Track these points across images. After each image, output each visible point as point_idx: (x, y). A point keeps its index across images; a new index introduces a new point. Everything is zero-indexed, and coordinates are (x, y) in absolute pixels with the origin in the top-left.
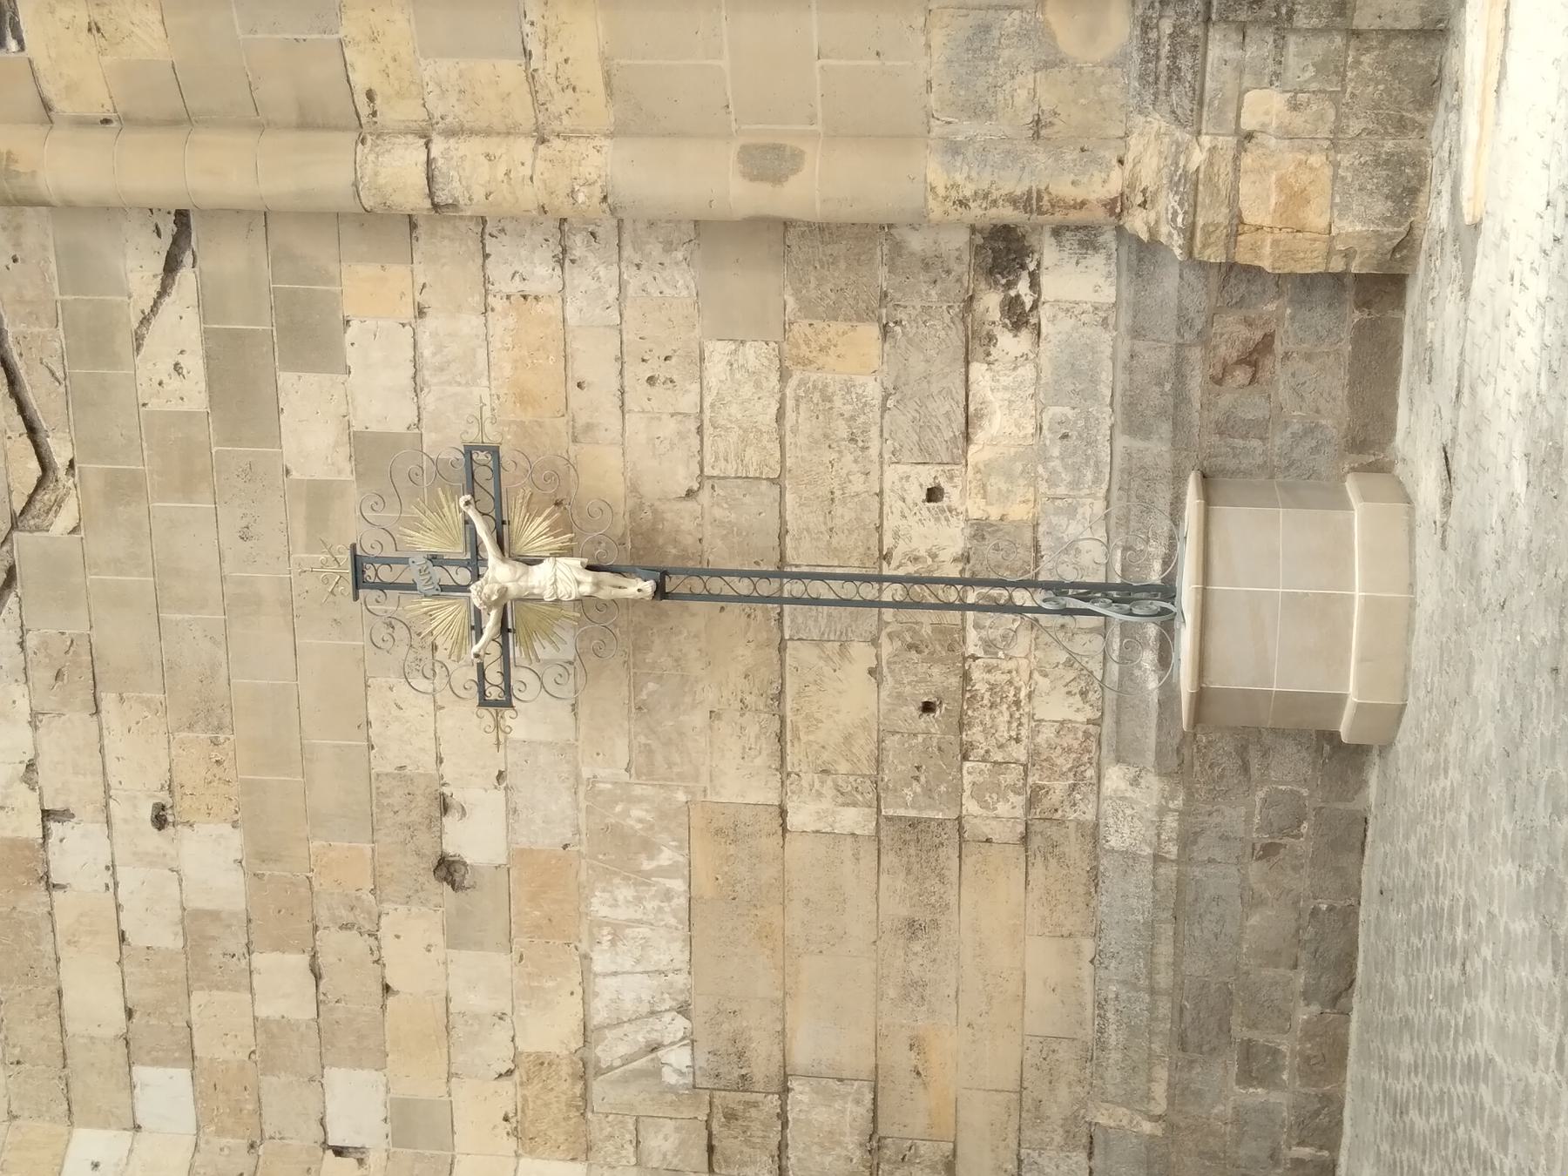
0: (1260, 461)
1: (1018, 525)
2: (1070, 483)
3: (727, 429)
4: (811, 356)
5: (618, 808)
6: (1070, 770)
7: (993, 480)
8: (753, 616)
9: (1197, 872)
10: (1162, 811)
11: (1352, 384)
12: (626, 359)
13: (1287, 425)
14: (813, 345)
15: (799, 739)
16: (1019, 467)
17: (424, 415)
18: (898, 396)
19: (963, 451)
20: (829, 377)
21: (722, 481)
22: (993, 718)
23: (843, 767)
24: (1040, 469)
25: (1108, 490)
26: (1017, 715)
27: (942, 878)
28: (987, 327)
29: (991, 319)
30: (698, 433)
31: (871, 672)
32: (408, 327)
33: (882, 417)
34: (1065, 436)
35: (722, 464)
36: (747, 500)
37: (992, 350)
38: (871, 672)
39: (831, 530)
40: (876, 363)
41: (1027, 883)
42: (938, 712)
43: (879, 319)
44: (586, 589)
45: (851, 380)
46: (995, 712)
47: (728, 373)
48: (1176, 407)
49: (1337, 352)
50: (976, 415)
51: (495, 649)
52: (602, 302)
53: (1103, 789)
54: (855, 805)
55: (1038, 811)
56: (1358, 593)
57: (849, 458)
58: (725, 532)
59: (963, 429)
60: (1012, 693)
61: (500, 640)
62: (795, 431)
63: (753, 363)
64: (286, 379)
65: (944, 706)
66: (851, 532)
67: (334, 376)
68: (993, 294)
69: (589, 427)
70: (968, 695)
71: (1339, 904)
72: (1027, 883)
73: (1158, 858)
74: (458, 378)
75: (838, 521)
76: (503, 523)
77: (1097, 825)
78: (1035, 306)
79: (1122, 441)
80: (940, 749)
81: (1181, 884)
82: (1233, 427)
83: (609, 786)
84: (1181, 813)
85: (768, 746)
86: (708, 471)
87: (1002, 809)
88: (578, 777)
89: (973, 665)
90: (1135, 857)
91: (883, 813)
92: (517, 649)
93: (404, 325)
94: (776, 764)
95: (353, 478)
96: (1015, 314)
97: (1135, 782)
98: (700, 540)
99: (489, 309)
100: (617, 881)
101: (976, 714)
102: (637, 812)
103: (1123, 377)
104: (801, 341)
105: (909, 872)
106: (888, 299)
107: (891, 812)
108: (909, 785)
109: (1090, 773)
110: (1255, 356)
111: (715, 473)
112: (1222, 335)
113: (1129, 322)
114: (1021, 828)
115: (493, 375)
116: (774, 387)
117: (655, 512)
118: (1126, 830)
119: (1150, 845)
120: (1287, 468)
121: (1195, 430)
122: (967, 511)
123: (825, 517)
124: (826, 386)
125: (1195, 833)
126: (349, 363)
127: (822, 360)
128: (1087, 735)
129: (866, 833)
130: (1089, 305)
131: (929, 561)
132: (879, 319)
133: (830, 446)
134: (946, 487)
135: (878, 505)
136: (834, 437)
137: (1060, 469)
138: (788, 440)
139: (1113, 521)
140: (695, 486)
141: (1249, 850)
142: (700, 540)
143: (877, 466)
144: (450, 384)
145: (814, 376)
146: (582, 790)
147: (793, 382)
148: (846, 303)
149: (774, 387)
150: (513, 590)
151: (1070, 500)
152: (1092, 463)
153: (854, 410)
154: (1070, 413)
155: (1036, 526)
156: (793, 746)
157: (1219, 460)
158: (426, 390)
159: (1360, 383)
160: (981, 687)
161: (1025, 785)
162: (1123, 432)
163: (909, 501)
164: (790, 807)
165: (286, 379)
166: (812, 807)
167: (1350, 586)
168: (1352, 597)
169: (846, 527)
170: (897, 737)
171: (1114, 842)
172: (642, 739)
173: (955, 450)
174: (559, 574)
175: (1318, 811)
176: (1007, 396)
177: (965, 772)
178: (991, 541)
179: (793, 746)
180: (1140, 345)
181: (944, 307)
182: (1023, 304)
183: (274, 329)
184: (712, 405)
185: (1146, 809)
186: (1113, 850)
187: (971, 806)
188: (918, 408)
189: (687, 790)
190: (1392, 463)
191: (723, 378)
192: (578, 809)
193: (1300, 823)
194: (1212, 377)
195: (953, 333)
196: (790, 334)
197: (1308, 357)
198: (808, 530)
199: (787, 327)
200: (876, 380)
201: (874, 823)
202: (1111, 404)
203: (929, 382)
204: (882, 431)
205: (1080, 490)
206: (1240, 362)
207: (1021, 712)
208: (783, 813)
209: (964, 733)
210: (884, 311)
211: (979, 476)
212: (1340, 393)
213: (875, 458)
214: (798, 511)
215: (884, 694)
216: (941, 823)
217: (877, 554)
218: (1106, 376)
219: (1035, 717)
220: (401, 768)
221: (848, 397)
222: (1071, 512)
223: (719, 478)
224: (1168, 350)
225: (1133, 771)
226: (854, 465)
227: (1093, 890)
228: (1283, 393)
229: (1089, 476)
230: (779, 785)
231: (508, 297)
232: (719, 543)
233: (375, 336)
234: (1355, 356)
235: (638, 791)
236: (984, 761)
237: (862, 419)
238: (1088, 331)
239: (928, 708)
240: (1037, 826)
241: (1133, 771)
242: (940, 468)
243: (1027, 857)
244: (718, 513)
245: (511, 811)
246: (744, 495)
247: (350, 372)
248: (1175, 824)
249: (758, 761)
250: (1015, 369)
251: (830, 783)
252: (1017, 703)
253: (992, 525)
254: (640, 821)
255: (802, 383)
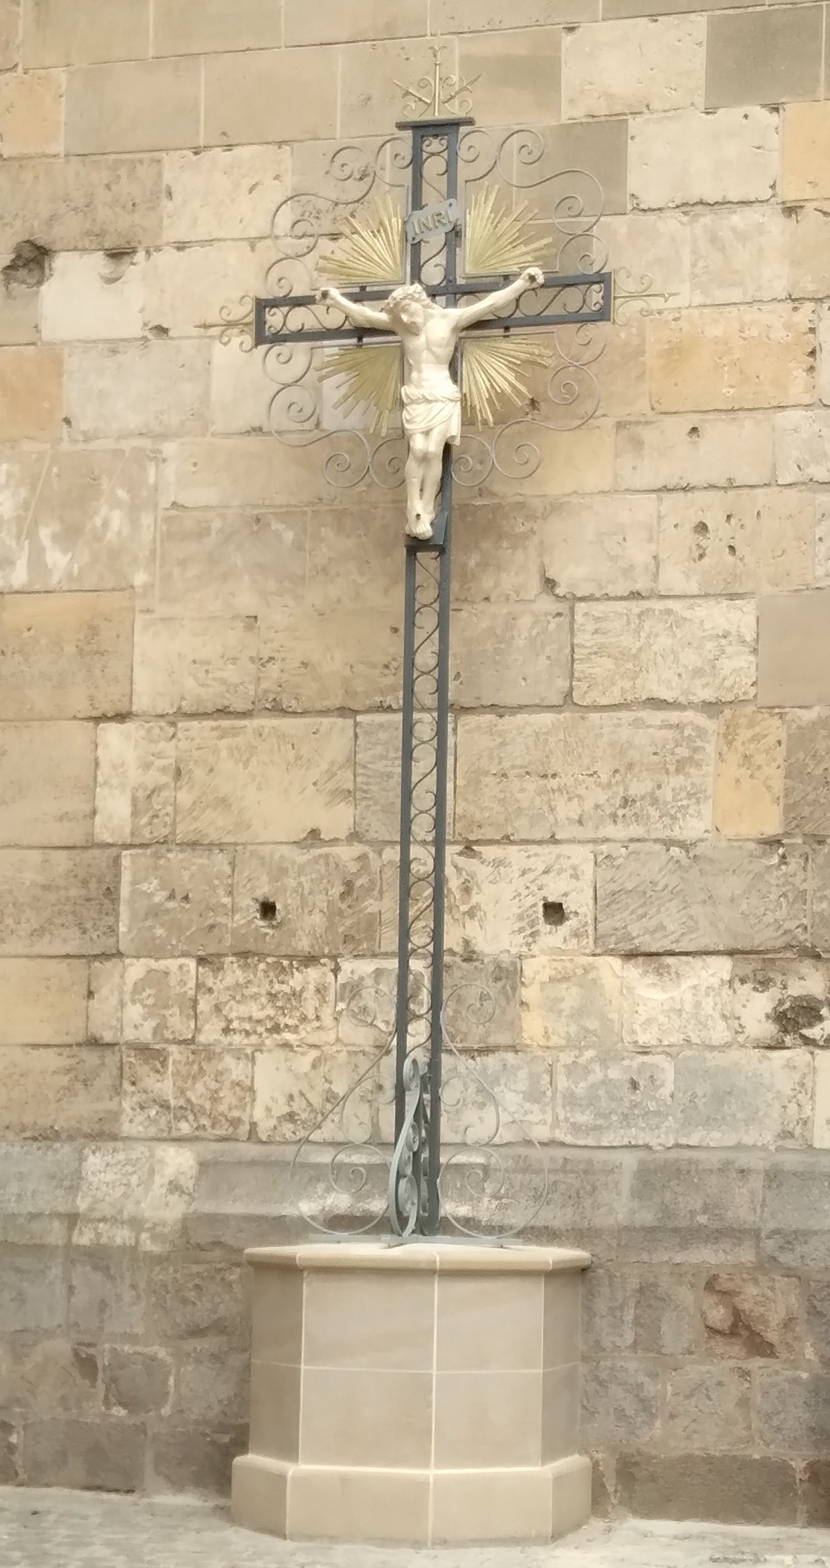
0: (606, 1342)
1: (514, 1026)
2: (572, 1093)
3: (637, 632)
4: (737, 744)
5: (122, 494)
6: (189, 1101)
7: (575, 990)
8: (386, 671)
9: (56, 1271)
10: (136, 1223)
11: (709, 1460)
12: (731, 493)
13: (654, 1376)
14: (752, 746)
15: (221, 737)
16: (593, 1024)
17: (651, 217)
18: (685, 862)
19: (612, 950)
20: (711, 769)
21: (566, 627)
22: (255, 997)
23: (185, 798)
24: (590, 1054)
25: (563, 1144)
26: (260, 1029)
27: (38, 933)
28: (779, 978)
29: (789, 983)
30: (632, 593)
31: (314, 834)
32: (770, 192)
33: (656, 841)
34: (634, 1085)
35: (591, 626)
36: (543, 661)
37: (749, 986)
38: (314, 834)
39: (504, 775)
40: (729, 831)
41: (35, 1046)
42: (262, 923)
43: (787, 834)
44: (418, 443)
45: (707, 798)
46: (264, 1000)
47: (714, 632)
48: (676, 1230)
49: (750, 1441)
50: (661, 966)
51: (333, 320)
52: (807, 457)
53: (164, 1146)
54: (135, 814)
55: (132, 1060)
56: (432, 1473)
57: (601, 797)
58: (499, 631)
59: (644, 949)
60: (290, 1022)
61: (347, 326)
62: (637, 724)
63: (727, 665)
64: (698, 25)
65: (270, 931)
66: (502, 801)
67: (702, 92)
68: (823, 985)
69: (637, 444)
70: (285, 963)
71: (17, 1458)
72: (35, 1046)
73: (72, 1219)
74: (701, 264)
75: (515, 785)
76: (507, 329)
77: (114, 1138)
78: (808, 1041)
79: (629, 1161)
80: (212, 927)
81: (39, 1250)
82: (650, 1306)
83: (152, 480)
84: (134, 1249)
85: (211, 696)
86: (581, 607)
87: (134, 1012)
88: (163, 436)
89: (326, 969)
90: (73, 1189)
91: (125, 853)
92: (336, 350)
93: (773, 187)
94: (186, 706)
95: (564, 120)
96: (798, 1014)
97: (174, 1187)
98: (487, 599)
99: (796, 304)
100: (23, 493)
101: (260, 974)
102: (117, 519)
103: (714, 1160)
104: (757, 729)
105: (46, 888)
106: (816, 846)
107: (126, 862)
108: (162, 887)
109: (185, 1128)
110: (745, 1333)
111: (579, 618)
112: (772, 1289)
113: (787, 1167)
114: (108, 1037)
115: (706, 310)
116: (694, 695)
117: (525, 537)
118: (109, 1177)
119: (91, 1209)
120: (596, 1379)
121: (645, 1257)
122: (533, 956)
123: (521, 767)
124: (698, 765)
125: (107, 1268)
126: (721, 111)
127: (733, 759)
128: (235, 1123)
129: (97, 830)
130: (809, 1113)
131: (464, 908)
132: (787, 834)
133: (616, 771)
134: (564, 929)
135: (538, 836)
136: (629, 776)
137: (592, 1079)
138: (626, 716)
139: (523, 1151)
140: (560, 591)
141: (87, 1339)
142: (487, 599)
143: (591, 835)
144: (694, 252)
145: (710, 749)
146: (146, 443)
147: (702, 720)
148: (810, 789)
149: (694, 695)
150: (416, 343)
151: (549, 1093)
152: (600, 1122)
153: (666, 803)
154: (665, 1092)
155: (513, 1049)
156: (213, 729)
157: (605, 1290)
158: (685, 219)
159: (710, 1471)
160: (296, 980)
161: (167, 1041)
162: (641, 1163)
163: (545, 879)
164: (129, 726)
165: (698, 25)
166: (131, 757)
167: (440, 1464)
168: (426, 1465)
169: (508, 795)
170: (227, 869)
171: (94, 1161)
172: (216, 524)
173: (613, 939)
174: (438, 406)
175: (141, 1429)
176: (688, 1007)
177: (182, 960)
178: (493, 990)
179: (213, 729)
180: (757, 1182)
181: (805, 921)
182: (811, 1025)
183: (766, 8)
184: (669, 612)
185: (138, 1203)
186: (81, 1159)
187: (136, 969)
188: (670, 888)
189: (148, 588)
190: (605, 1515)
191: (707, 626)
192: (120, 437)
193: (124, 1405)
194: (715, 1277)
195: (770, 933)
196: (767, 716)
197: (744, 1402)
198: (503, 744)
199: (777, 710)
200: (706, 831)
201: (110, 841)
202: (678, 1146)
203: (704, 902)
204: (638, 840)
205: (564, 1107)
206: (737, 1313)
207: (265, 1035)
208: (122, 717)
209: (234, 959)
210: (799, 840)
211: (580, 972)
212: (697, 1445)
213: (601, 834)
214: (528, 730)
215: (285, 850)
216: (113, 930)
217: (472, 837)
218: (715, 1138)
219: (257, 1054)
220: (170, 195)
221: (683, 794)
222: (533, 1096)
223: (572, 621)
224: (751, 1218)
225: (188, 1184)
226: (592, 805)
227: (28, 1134)
228: (695, 1371)
229: (583, 1118)
230: (159, 712)
231: (812, 330)
232: (485, 624)
233: (759, 148)
234: (745, 1464)
235: (147, 519)
236: (199, 986)
237: (654, 813)
238: (776, 1113)
239: (268, 909)
240: (111, 1059)
241: (188, 1184)
242: (590, 919)
243: (71, 1046)
244: (525, 622)
245: (114, 347)
246: (549, 658)
247: (708, 113)
248: (119, 1241)
249: (190, 684)
250: (724, 1017)
251: (164, 779)
252: (276, 1029)
253: (514, 989)
254: (106, 524)
255: (701, 732)
